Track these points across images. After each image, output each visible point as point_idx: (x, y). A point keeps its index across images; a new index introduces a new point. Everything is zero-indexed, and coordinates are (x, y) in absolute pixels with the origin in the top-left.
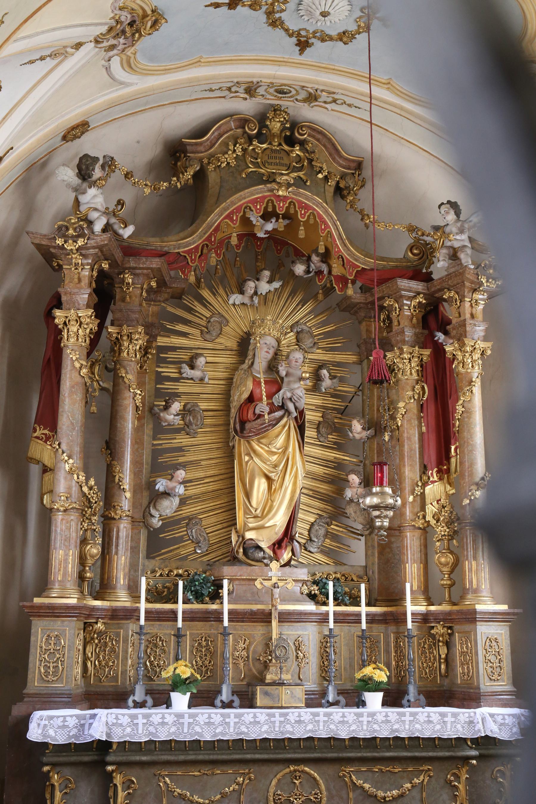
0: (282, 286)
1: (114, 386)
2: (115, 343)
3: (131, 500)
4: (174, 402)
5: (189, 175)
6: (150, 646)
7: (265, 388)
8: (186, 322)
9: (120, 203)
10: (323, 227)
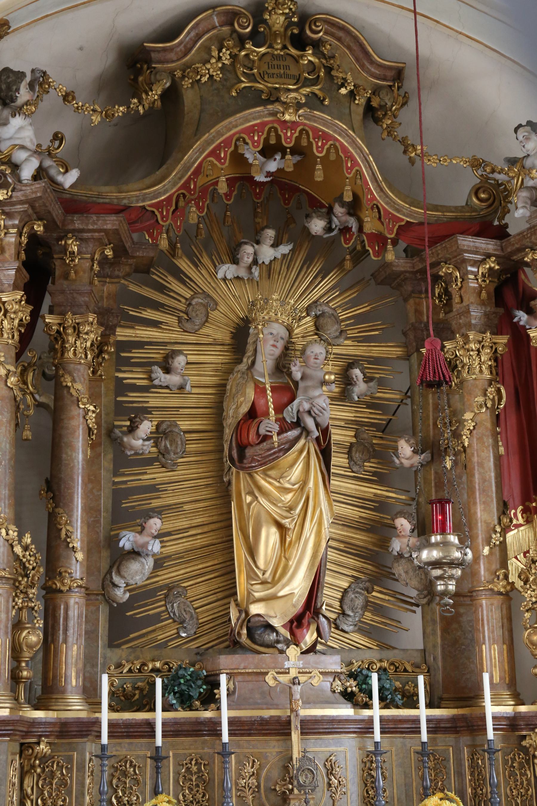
1: (56, 400)
2: (56, 339)
3: (85, 563)
4: (142, 421)
5: (155, 94)
6: (117, 774)
7: (272, 397)
8: (157, 306)
9: (58, 137)
10: (349, 165)
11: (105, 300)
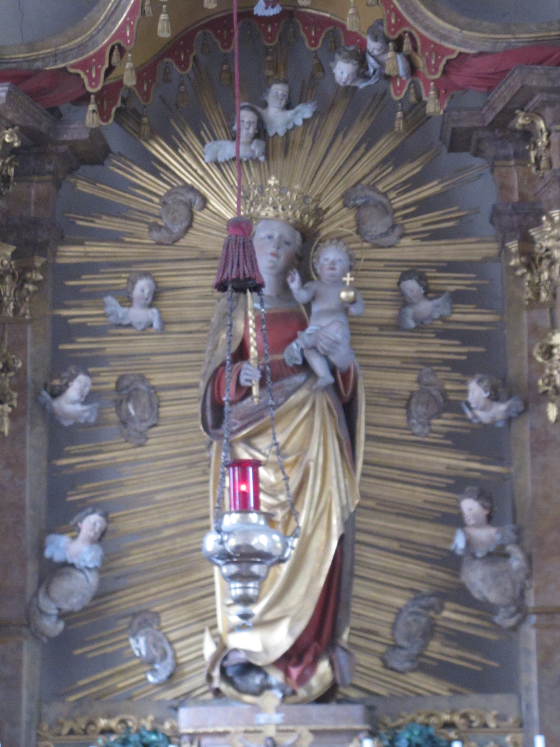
0: (315, 114)
11: (32, 207)
